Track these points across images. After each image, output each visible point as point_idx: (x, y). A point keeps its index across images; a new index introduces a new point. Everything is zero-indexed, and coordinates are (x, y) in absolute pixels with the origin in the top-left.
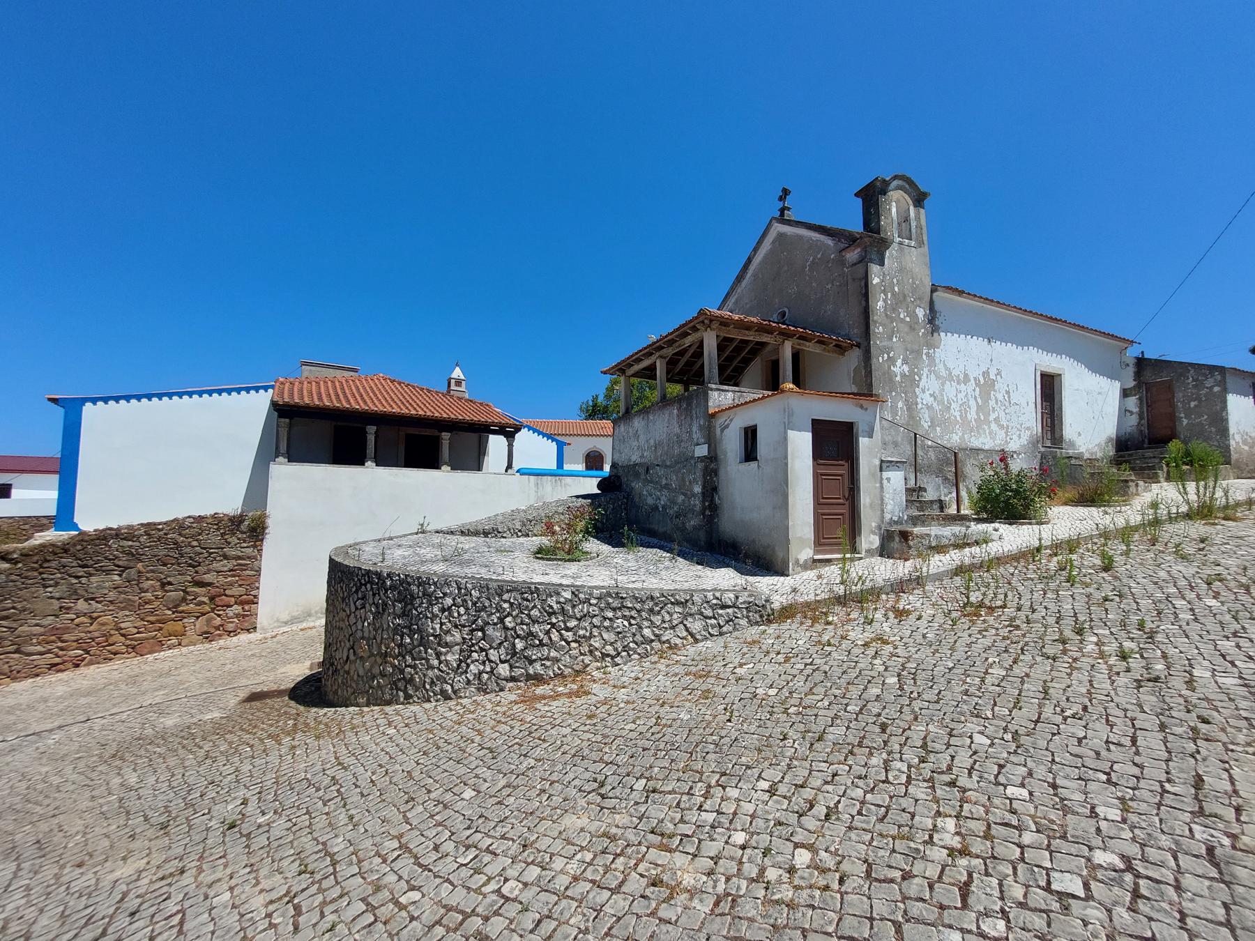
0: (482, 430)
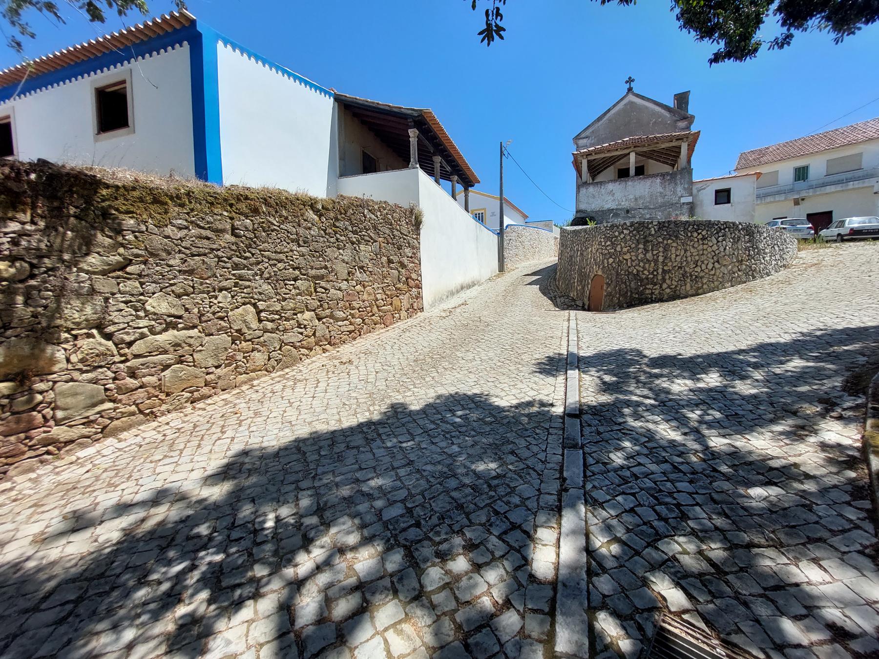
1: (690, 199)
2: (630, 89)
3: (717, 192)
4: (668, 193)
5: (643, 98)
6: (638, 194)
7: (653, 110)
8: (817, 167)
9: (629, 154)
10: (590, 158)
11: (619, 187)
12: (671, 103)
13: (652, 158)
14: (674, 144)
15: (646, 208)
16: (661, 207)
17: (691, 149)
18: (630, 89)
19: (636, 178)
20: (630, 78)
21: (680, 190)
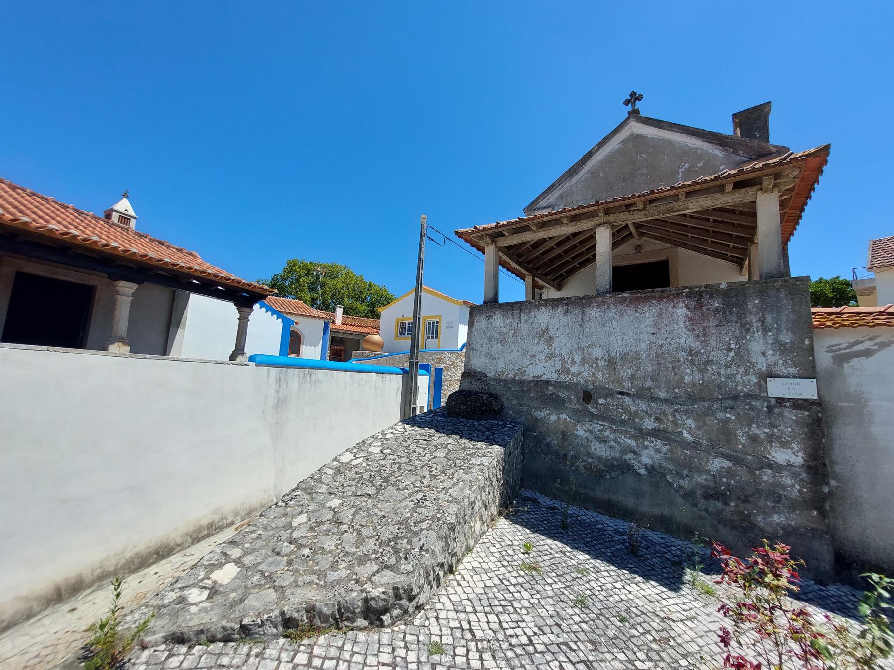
0: (177, 283)
1: (807, 389)
4: (718, 355)
6: (617, 348)
10: (504, 242)
11: (564, 319)
12: (727, 129)
13: (686, 246)
14: (729, 199)
15: (640, 394)
16: (693, 398)
17: (791, 216)
18: (634, 113)
20: (633, 94)
21: (761, 349)
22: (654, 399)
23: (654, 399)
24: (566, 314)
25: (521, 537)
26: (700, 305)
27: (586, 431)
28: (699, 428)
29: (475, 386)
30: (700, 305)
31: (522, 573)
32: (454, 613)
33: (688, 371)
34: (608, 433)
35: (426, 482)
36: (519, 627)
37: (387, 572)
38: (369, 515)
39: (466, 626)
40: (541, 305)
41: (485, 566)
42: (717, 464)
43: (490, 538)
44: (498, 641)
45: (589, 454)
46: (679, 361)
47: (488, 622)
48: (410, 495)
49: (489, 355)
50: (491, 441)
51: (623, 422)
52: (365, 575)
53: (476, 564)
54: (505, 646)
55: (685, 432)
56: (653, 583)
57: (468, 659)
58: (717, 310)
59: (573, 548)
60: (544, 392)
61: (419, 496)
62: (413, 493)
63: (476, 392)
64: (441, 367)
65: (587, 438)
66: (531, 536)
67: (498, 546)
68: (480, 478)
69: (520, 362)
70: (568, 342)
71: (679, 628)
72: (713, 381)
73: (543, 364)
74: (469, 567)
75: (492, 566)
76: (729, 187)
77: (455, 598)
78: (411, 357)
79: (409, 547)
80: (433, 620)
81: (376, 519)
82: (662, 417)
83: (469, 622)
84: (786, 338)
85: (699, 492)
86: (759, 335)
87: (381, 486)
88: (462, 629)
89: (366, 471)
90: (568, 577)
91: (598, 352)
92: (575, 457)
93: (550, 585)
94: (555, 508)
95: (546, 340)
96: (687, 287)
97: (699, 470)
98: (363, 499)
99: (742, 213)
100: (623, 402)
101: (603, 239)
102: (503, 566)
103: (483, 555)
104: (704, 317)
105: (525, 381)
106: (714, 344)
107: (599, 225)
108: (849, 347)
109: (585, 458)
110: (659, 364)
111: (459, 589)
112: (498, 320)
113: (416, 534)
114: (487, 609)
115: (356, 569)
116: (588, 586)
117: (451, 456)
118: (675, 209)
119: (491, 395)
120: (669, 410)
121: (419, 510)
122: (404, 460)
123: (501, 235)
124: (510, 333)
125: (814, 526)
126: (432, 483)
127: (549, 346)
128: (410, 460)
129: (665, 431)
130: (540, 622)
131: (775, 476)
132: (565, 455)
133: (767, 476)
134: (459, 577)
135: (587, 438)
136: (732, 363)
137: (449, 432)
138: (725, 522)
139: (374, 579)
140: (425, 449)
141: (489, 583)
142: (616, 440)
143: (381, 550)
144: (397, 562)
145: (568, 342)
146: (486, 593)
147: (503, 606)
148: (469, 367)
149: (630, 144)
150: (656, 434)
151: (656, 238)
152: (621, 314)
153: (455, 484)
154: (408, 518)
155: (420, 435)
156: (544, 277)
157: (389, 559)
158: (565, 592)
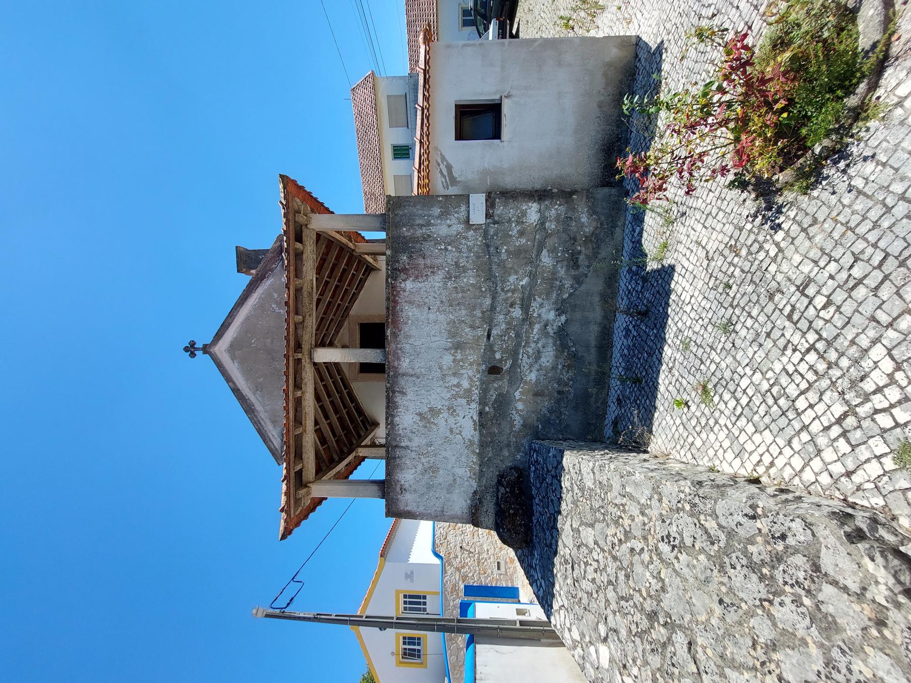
1: (478, 202)
2: (206, 349)
3: (460, 135)
4: (451, 257)
5: (225, 326)
7: (255, 308)
8: (394, 136)
9: (315, 364)
11: (411, 395)
12: (245, 279)
13: (348, 309)
15: (489, 318)
16: (490, 277)
18: (206, 349)
19: (391, 347)
20: (186, 349)
22: (493, 308)
23: (493, 308)
24: (404, 394)
25: (668, 418)
26: (405, 270)
27: (531, 371)
28: (516, 273)
29: (489, 506)
30: (405, 270)
31: (716, 399)
32: (823, 454)
33: (465, 280)
34: (530, 350)
35: (638, 545)
36: (796, 370)
37: (827, 562)
38: (728, 634)
39: (836, 431)
40: (392, 421)
41: (726, 444)
42: (546, 259)
43: (682, 452)
44: (833, 383)
45: (554, 368)
46: (456, 288)
47: (811, 406)
48: (669, 564)
49: (450, 489)
50: (559, 468)
51: (518, 335)
52: (857, 608)
53: (730, 455)
54: (835, 373)
55: (521, 283)
56: (672, 286)
57: (892, 406)
58: (410, 257)
59: (660, 363)
60: (492, 416)
61: (665, 548)
62: (661, 559)
63: (497, 504)
64: (462, 586)
65: (538, 370)
66: (661, 409)
67: (690, 439)
68: (612, 466)
69: (459, 446)
70: (437, 410)
71: (712, 246)
72: (474, 262)
73: (460, 419)
74: (737, 463)
75: (722, 435)
76: (298, 245)
77: (797, 463)
78: (450, 630)
79: (759, 539)
80: (857, 478)
81: (732, 617)
82: (510, 301)
83: (827, 429)
84: (437, 211)
85: (573, 273)
86: (433, 229)
87: (665, 625)
88: (844, 434)
89: (646, 663)
90: (699, 353)
91: (447, 360)
92: (559, 382)
93: (718, 365)
94: (618, 400)
95: (433, 416)
96: (387, 280)
97: (554, 273)
98: (700, 655)
99: (326, 254)
100: (498, 335)
101: (325, 355)
102: (716, 422)
103: (711, 452)
104: (416, 267)
105: (480, 441)
106: (440, 261)
107: (311, 358)
108: (444, 176)
109: (559, 371)
110: (459, 304)
111: (780, 462)
112: (407, 477)
113: (731, 534)
114: (791, 414)
115: (852, 631)
116: (702, 332)
117: (589, 518)
118: (310, 290)
119: (499, 483)
120: (502, 296)
121: (688, 542)
122: (611, 594)
123: (299, 474)
124: (423, 460)
125: (585, 198)
126: (638, 533)
127: (439, 412)
128: (610, 582)
129: (522, 299)
130: (775, 352)
131: (550, 221)
132: (559, 392)
133: (551, 226)
134: (761, 470)
135: (538, 370)
136: (457, 248)
137: (553, 530)
138: (596, 254)
139: (854, 587)
140: (586, 564)
141: (750, 429)
142: (536, 342)
143: (788, 589)
144: (796, 551)
145: (437, 410)
146: (767, 427)
147: (776, 401)
148: (465, 516)
149: (238, 353)
150: (525, 307)
151: (337, 332)
152: (408, 337)
153: (631, 497)
154: (709, 557)
155: (566, 578)
156: (361, 438)
157: (797, 568)
158: (720, 347)
